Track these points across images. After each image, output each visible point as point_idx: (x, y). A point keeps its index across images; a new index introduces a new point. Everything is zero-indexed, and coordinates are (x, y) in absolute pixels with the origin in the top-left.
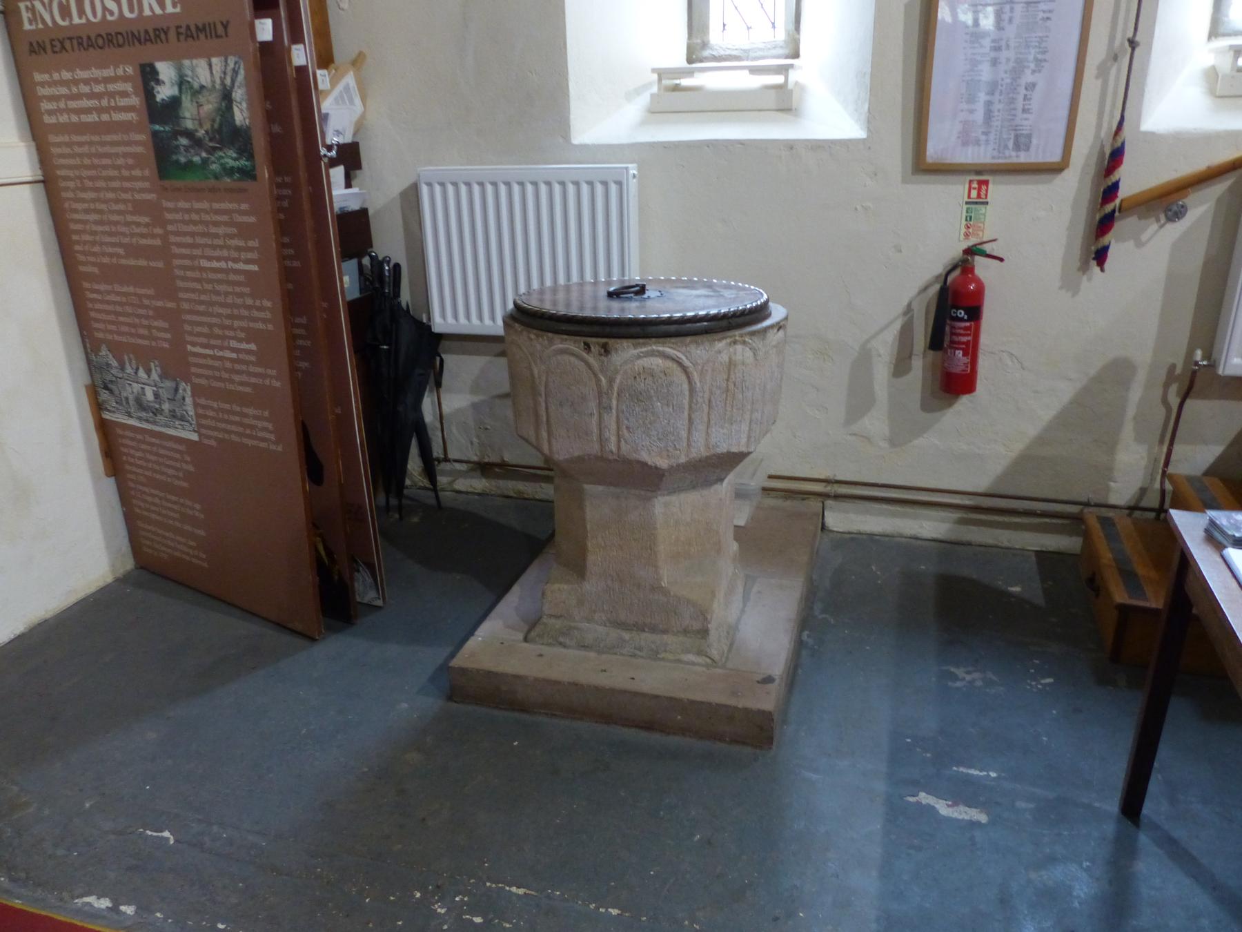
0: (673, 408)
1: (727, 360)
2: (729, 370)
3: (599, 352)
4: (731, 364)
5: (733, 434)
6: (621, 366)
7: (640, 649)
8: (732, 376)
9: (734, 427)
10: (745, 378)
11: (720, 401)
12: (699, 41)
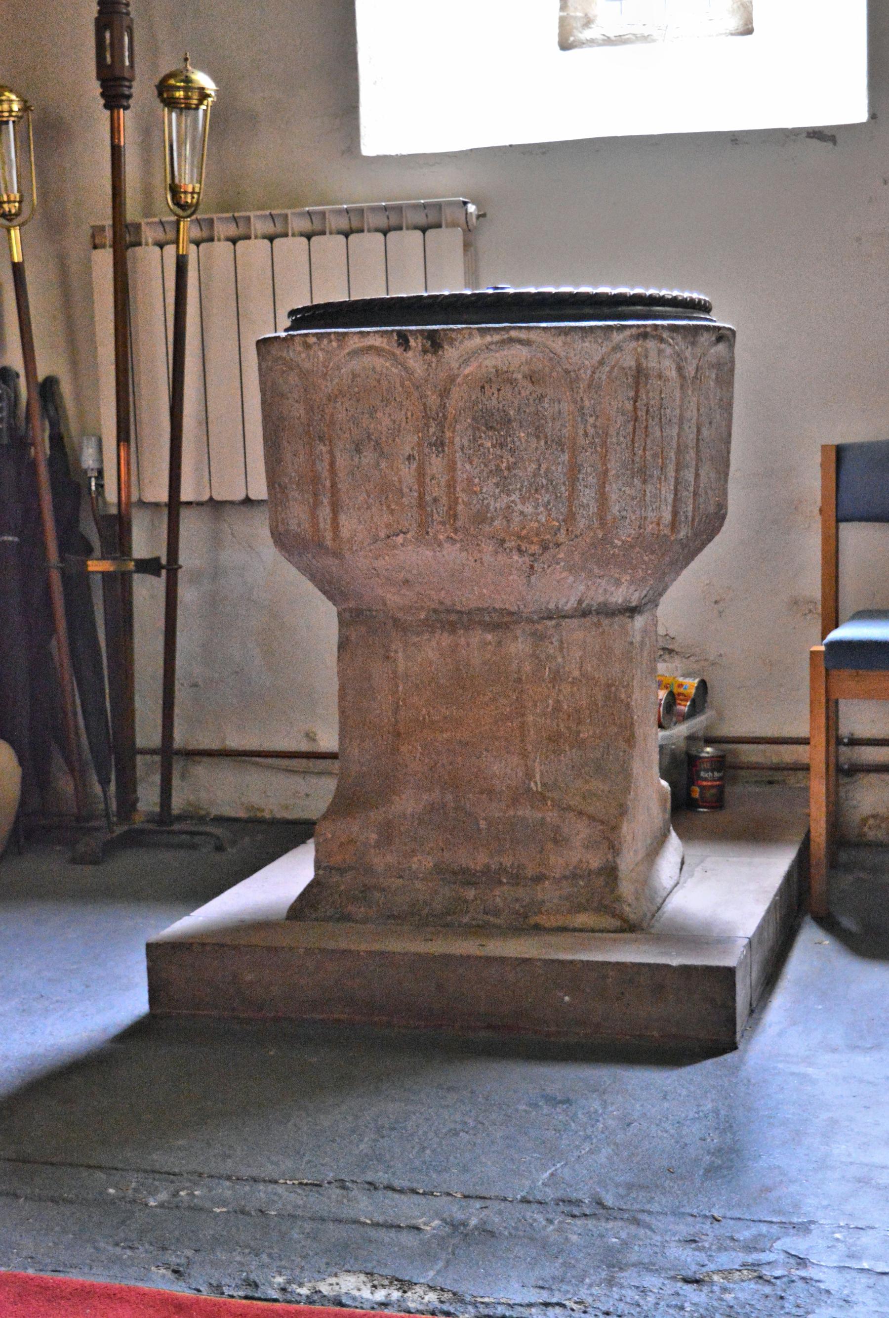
0: (546, 443)
1: (633, 364)
2: (637, 384)
3: (423, 345)
4: (640, 375)
5: (648, 498)
6: (459, 369)
7: (496, 913)
8: (642, 393)
9: (649, 488)
10: (664, 402)
11: (625, 437)
12: (579, 14)
